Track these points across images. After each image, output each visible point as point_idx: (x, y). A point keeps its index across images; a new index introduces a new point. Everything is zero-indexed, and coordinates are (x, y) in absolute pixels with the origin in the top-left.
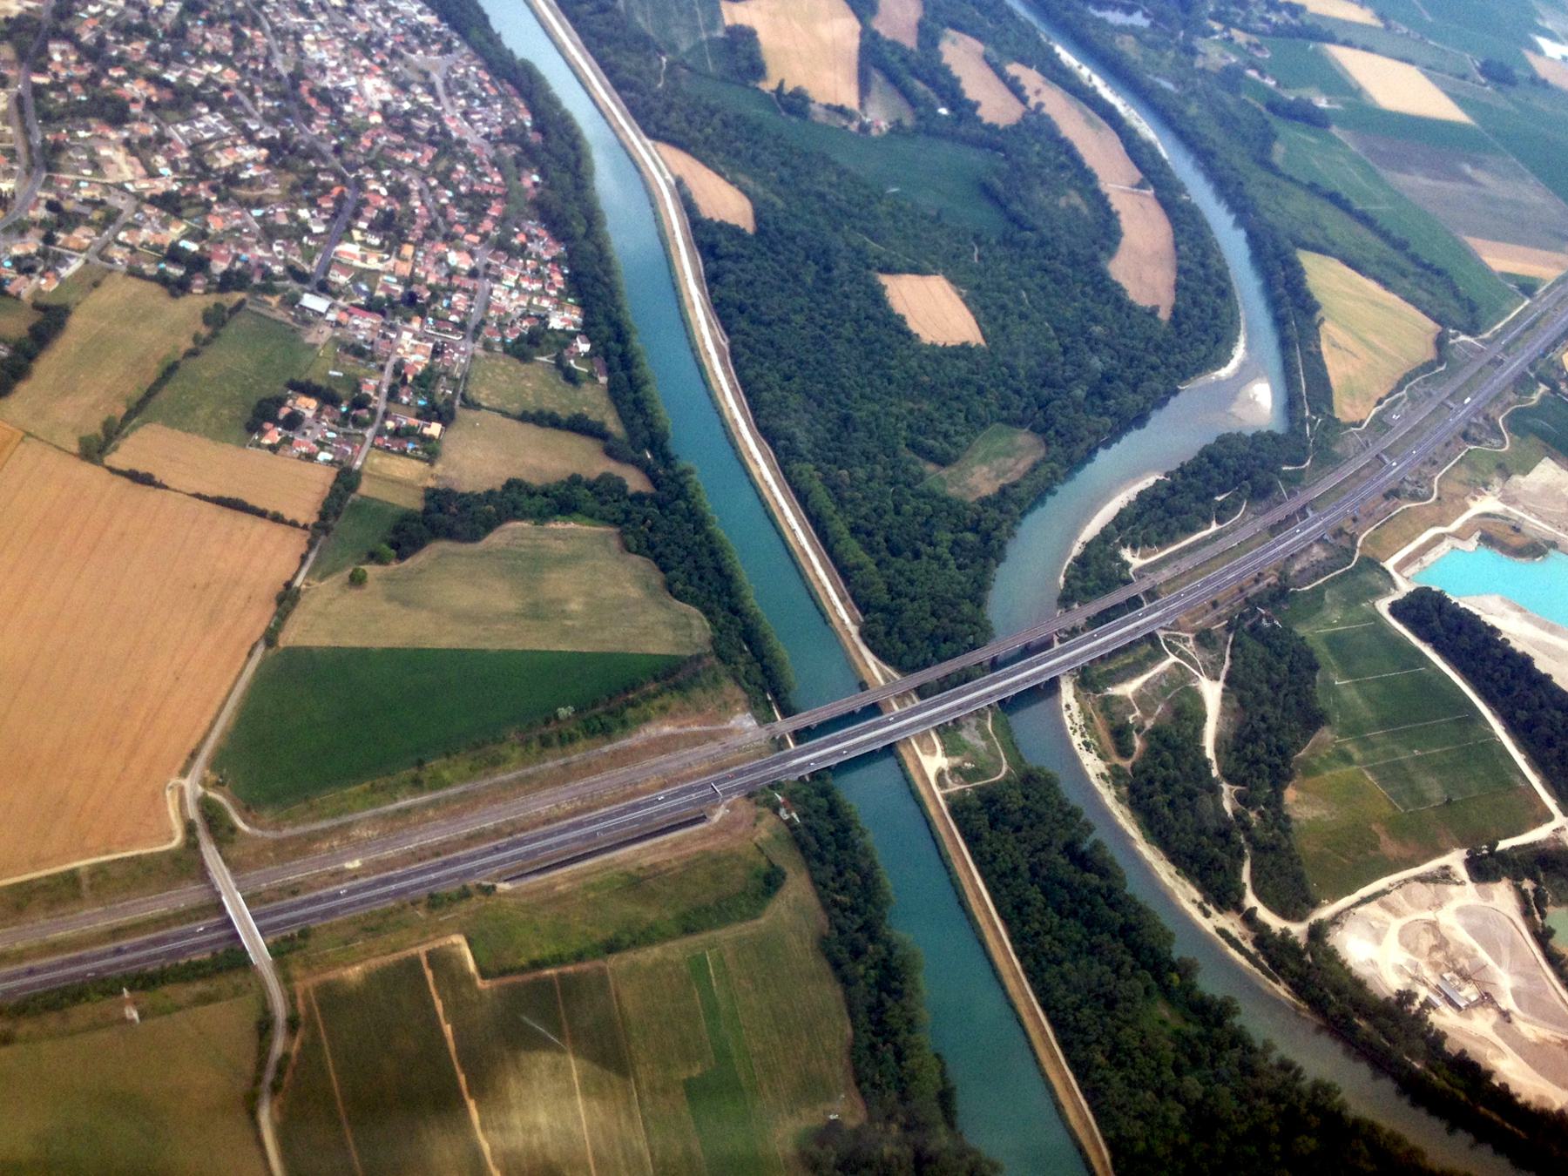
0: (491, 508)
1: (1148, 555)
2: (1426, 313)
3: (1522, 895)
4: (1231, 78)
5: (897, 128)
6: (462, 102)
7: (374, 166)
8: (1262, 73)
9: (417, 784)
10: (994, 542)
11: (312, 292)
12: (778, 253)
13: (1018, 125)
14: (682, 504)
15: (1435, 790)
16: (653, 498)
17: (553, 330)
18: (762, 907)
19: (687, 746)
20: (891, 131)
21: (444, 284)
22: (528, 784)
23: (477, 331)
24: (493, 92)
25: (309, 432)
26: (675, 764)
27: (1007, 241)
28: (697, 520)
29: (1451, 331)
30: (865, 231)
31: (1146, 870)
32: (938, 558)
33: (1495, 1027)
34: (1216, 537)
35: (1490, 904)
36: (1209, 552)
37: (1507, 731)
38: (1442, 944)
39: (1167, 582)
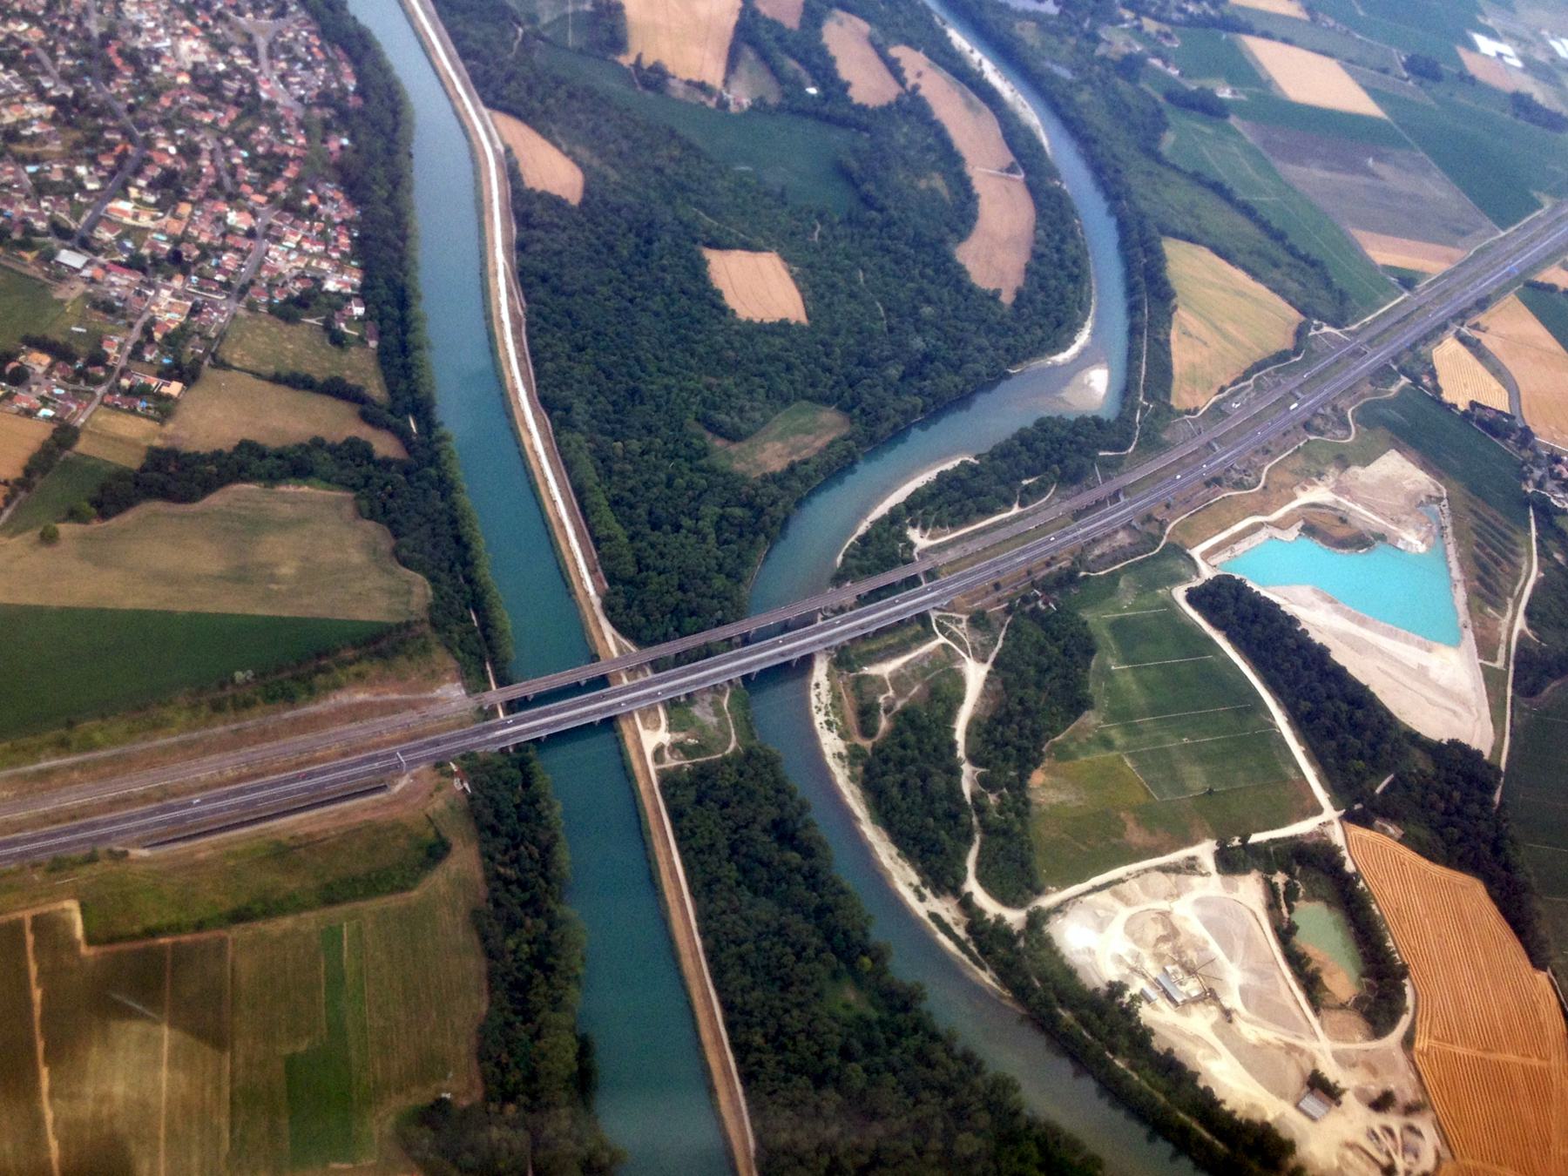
0: (213, 468)
1: (940, 536)
2: (1291, 303)
3: (1271, 889)
4: (1129, 67)
5: (759, 107)
6: (283, 65)
7: (167, 125)
8: (1166, 62)
9: (63, 746)
10: (767, 518)
11: (72, 249)
12: (598, 225)
13: (889, 106)
14: (433, 471)
15: (1196, 778)
16: (400, 462)
17: (327, 292)
18: (416, 880)
19: (382, 715)
20: (752, 108)
21: (217, 243)
22: (189, 749)
23: (243, 290)
24: (320, 56)
25: (34, 388)
26: (362, 733)
27: (850, 220)
28: (445, 487)
29: (1315, 322)
30: (699, 205)
31: (864, 851)
32: (697, 532)
33: (1214, 1027)
34: (1019, 517)
35: (1235, 896)
36: (1002, 534)
37: (1289, 723)
38: (1172, 934)
39: (950, 564)
